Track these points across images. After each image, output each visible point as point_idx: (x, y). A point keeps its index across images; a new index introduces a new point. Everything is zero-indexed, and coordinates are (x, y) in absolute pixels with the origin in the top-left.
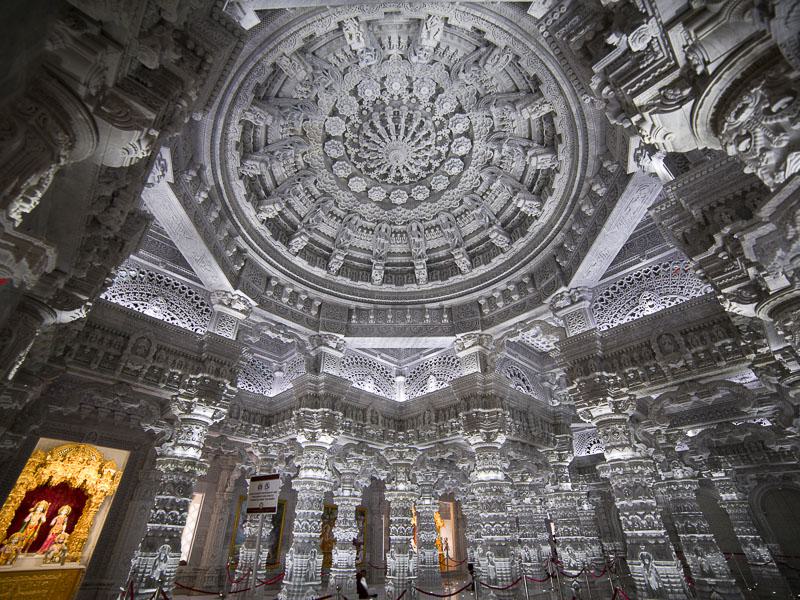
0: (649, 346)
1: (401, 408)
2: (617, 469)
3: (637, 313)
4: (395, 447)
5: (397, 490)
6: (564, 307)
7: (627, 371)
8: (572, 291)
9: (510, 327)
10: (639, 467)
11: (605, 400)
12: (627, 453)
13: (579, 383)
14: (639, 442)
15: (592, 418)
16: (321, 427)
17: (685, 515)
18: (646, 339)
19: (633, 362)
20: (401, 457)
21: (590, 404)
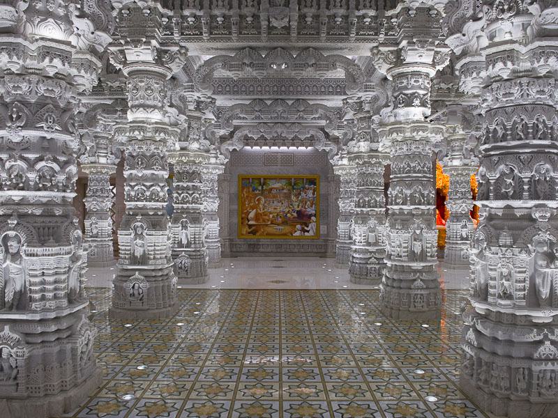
2: (137, 133)
10: (162, 135)
11: (148, 43)
12: (156, 116)
15: (125, 63)
17: (372, 190)
21: (127, 43)
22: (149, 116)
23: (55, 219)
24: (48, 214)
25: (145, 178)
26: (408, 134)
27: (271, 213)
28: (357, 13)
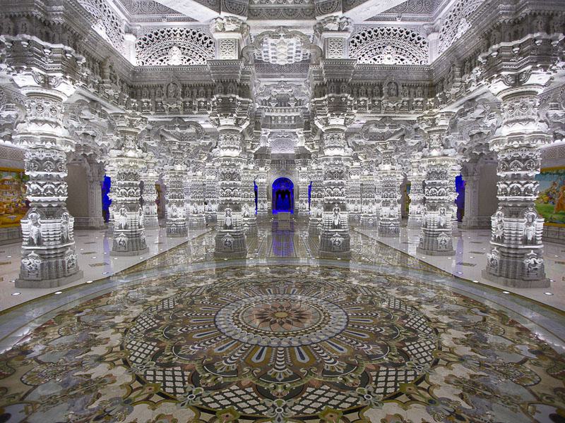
0: (380, 86)
1: (134, 73)
3: (165, 60)
4: (425, 115)
5: (126, 157)
6: (332, 31)
7: (143, 100)
8: (345, 19)
9: (272, 27)
11: (232, 115)
13: (218, 99)
14: (349, 147)
16: (63, 72)
18: (380, 81)
19: (367, 94)
20: (131, 125)
22: (233, 153)
23: (53, 209)
24: (50, 206)
25: (230, 185)
26: (127, 163)
27: (4, 203)
28: (415, 99)
